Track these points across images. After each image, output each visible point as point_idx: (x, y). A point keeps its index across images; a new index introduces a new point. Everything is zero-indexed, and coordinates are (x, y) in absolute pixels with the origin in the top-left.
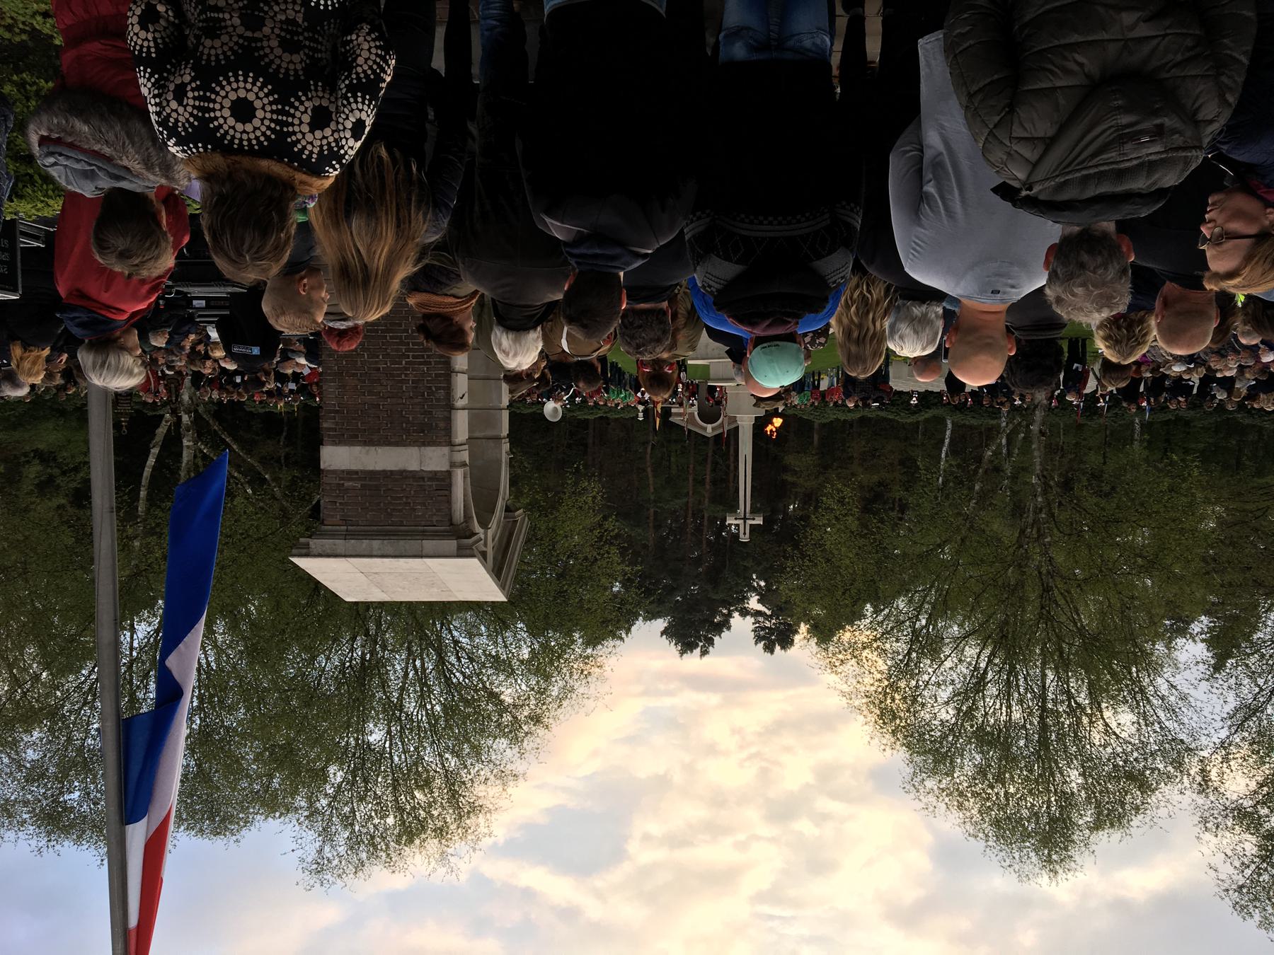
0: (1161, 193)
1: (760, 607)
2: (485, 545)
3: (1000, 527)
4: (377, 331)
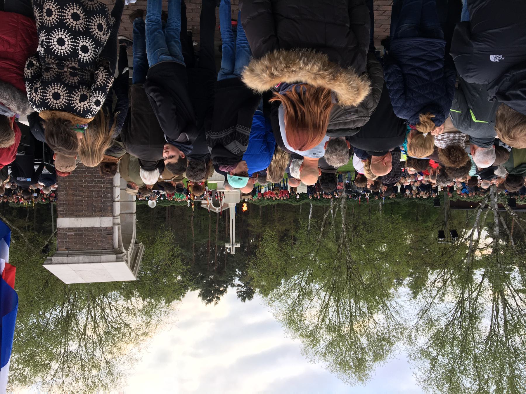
0: (358, 129)
1: (240, 283)
2: (127, 257)
3: (331, 245)
4: (82, 171)
